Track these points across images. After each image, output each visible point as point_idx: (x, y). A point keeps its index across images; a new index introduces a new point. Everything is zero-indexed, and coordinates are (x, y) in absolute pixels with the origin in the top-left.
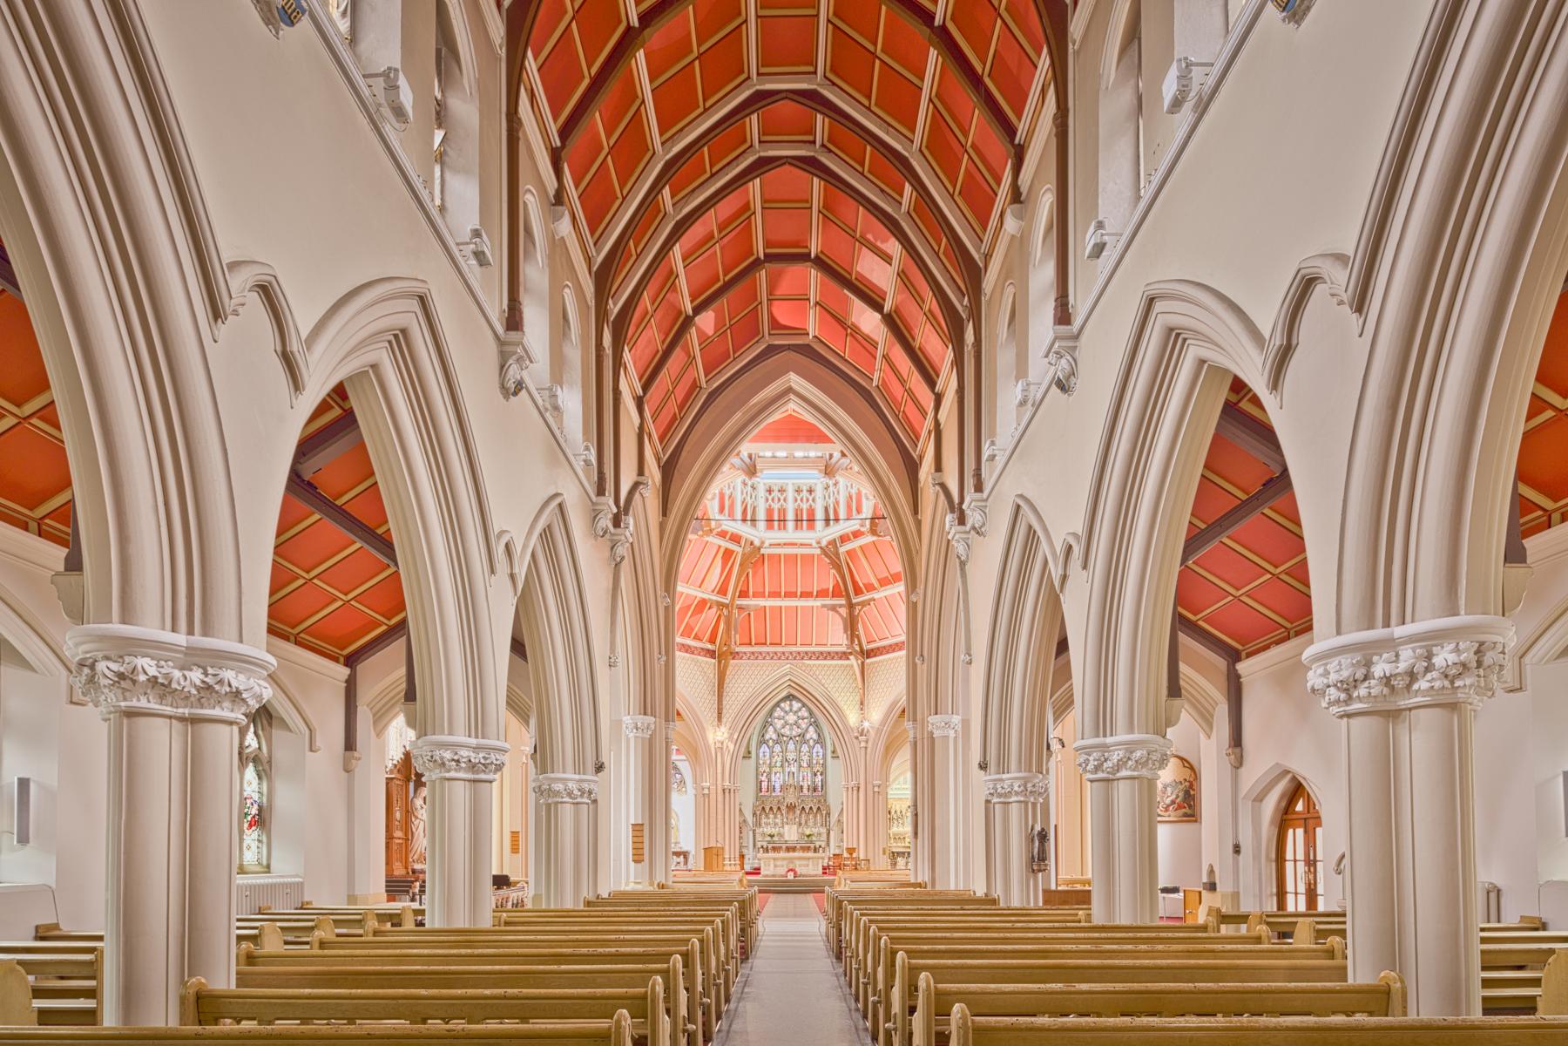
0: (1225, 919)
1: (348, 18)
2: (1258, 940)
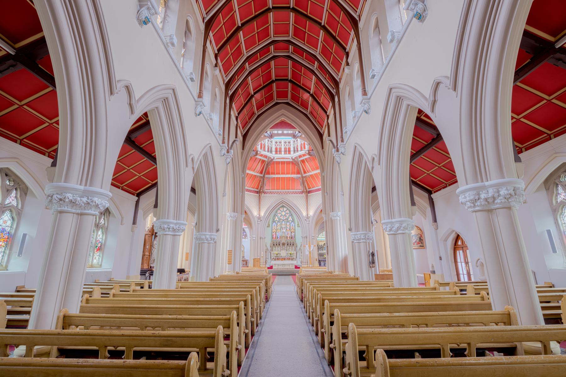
0: (441, 284)
1: (162, 24)
2: (455, 293)
